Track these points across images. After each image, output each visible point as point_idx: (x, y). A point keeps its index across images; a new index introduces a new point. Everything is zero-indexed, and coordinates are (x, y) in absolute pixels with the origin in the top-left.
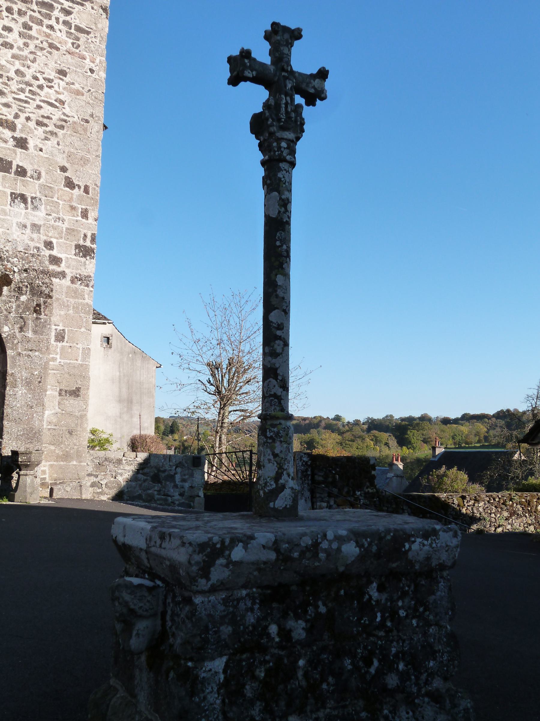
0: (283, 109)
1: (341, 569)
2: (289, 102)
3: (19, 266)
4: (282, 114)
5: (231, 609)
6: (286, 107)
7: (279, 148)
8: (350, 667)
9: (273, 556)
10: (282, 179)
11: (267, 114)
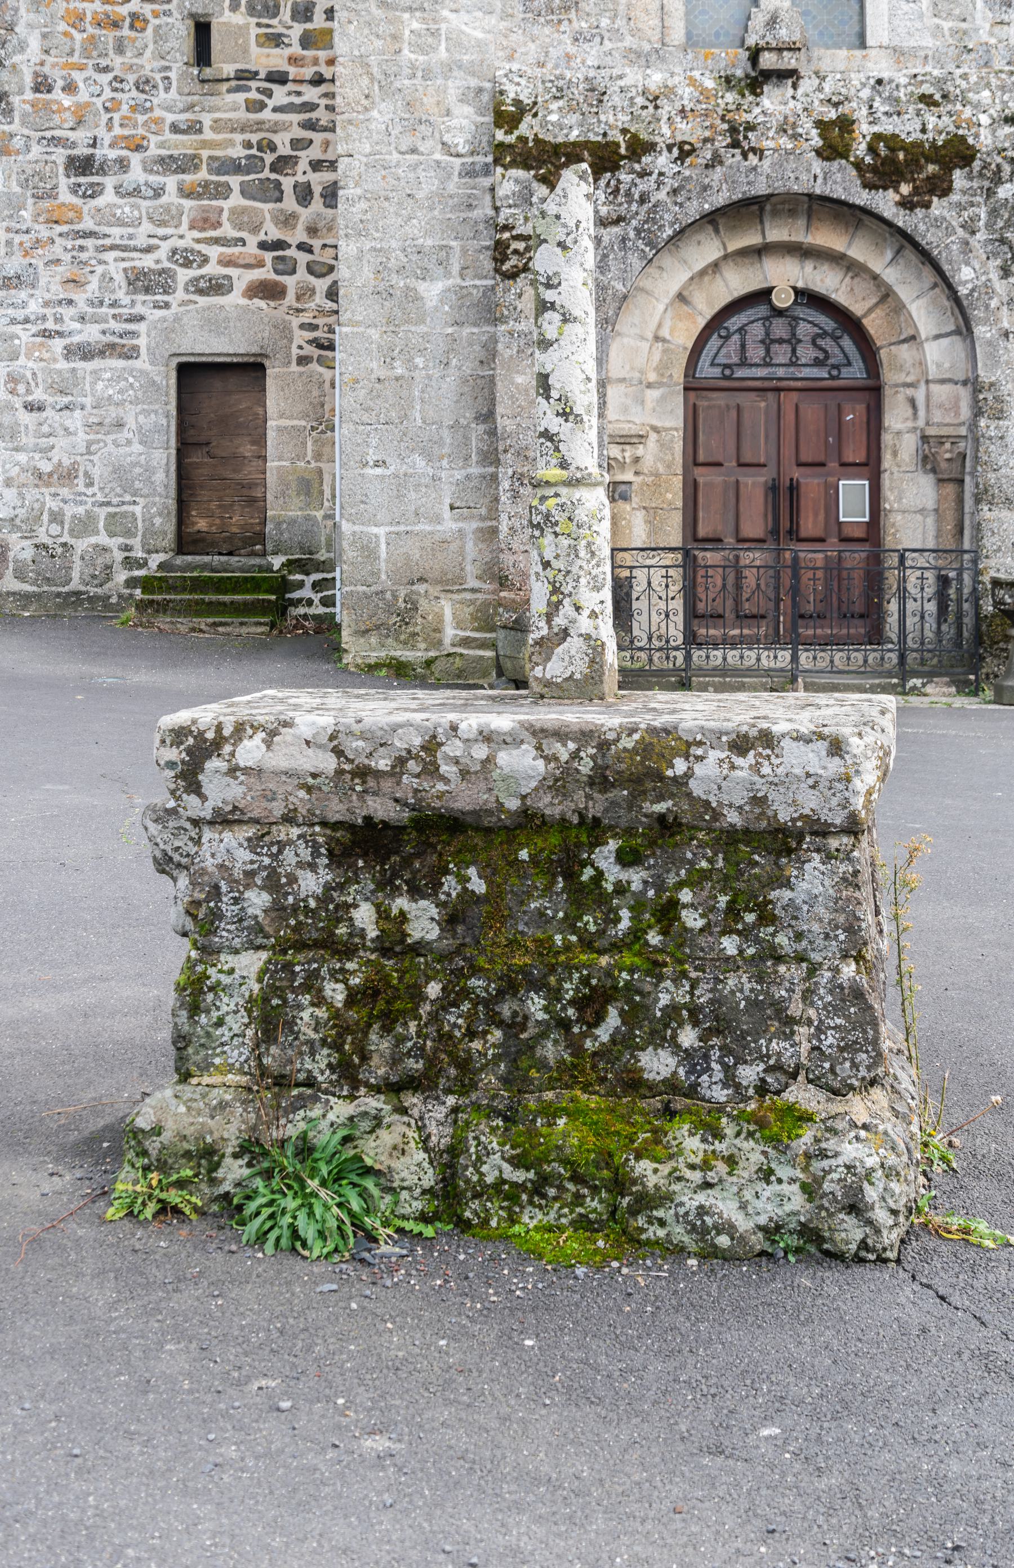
1: (513, 804)
3: (992, 111)
5: (267, 861)
8: (541, 1016)
9: (329, 763)
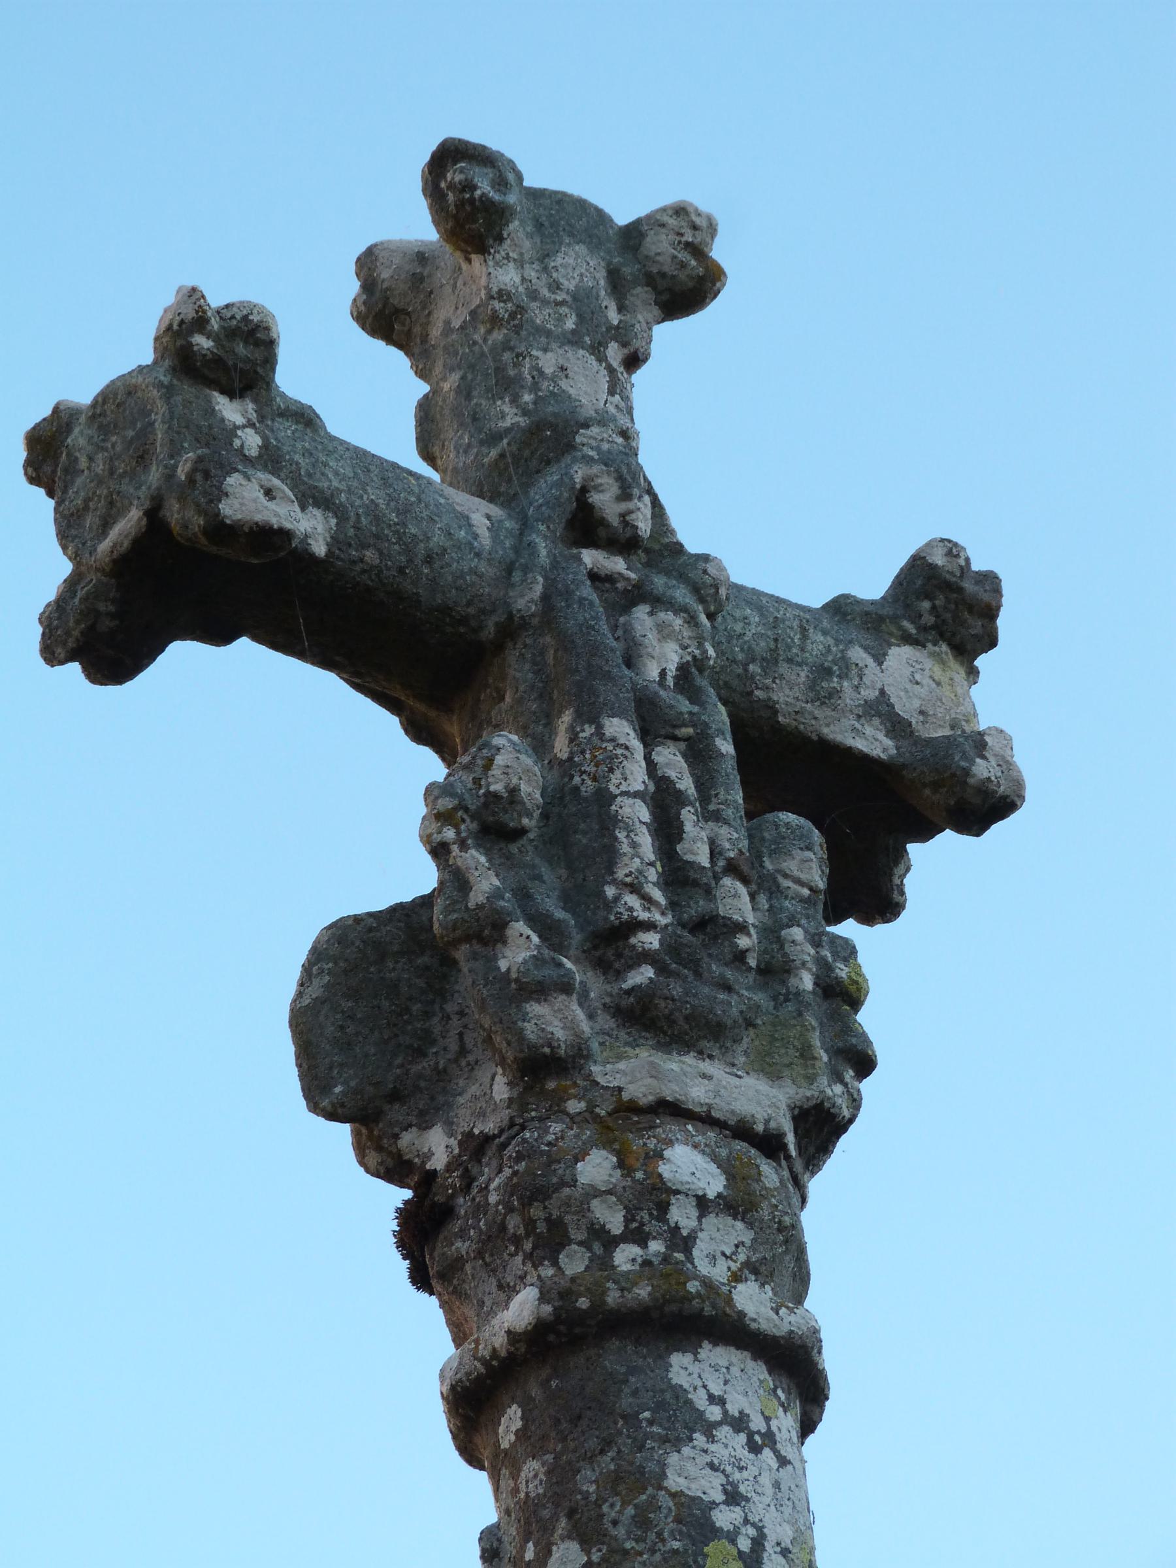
0: (639, 848)
2: (686, 784)
4: (635, 888)
6: (667, 831)
7: (651, 1198)
10: (725, 1518)
11: (486, 882)
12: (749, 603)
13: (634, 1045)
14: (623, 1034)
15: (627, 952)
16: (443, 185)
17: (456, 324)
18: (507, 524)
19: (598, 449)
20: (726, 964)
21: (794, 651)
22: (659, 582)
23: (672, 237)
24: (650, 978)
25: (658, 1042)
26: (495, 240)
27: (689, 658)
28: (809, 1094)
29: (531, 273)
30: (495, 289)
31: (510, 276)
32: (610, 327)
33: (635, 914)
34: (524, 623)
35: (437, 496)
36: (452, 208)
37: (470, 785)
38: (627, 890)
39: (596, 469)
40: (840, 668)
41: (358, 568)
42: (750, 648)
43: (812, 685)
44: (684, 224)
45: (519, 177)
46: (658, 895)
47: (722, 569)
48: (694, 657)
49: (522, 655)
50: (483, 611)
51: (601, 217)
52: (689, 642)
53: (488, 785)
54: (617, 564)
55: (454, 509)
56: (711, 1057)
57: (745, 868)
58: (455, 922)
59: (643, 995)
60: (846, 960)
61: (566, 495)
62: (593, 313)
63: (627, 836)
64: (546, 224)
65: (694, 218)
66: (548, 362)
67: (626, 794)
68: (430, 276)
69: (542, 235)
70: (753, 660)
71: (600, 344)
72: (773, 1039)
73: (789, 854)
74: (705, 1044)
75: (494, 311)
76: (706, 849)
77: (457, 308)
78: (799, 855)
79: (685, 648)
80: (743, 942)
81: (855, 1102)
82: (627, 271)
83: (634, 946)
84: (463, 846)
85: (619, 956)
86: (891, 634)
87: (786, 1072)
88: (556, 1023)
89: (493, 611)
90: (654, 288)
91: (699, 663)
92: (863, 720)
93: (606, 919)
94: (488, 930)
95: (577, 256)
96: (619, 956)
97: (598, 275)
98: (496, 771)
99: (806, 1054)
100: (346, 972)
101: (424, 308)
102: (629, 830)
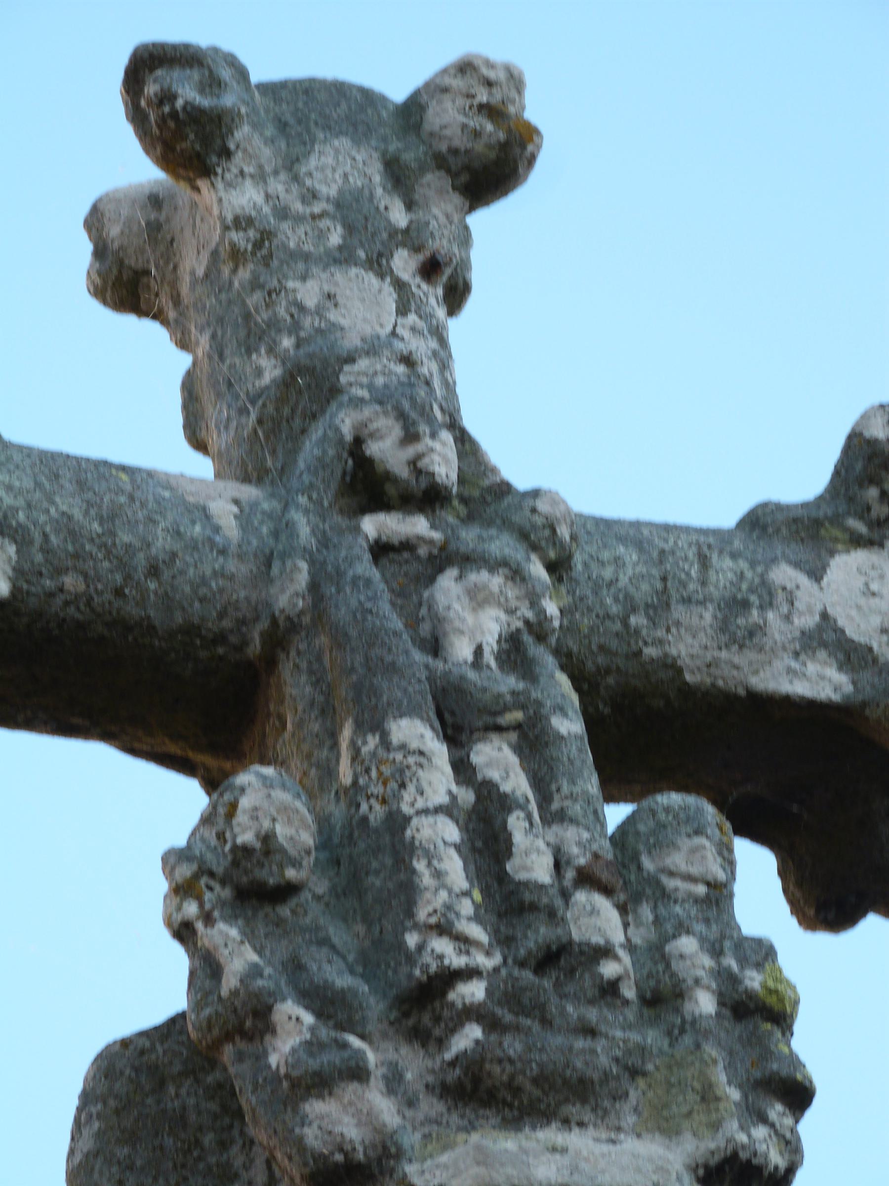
2: (516, 782)
4: (443, 929)
12: (622, 540)
13: (470, 1128)
14: (455, 1119)
15: (446, 1013)
16: (143, 103)
17: (200, 272)
18: (266, 506)
19: (371, 387)
20: (591, 1002)
21: (692, 586)
22: (469, 537)
23: (460, 101)
24: (477, 1042)
25: (504, 1119)
26: (219, 156)
27: (520, 624)
28: (712, 1146)
29: (277, 186)
30: (229, 217)
31: (248, 196)
32: (394, 232)
33: (446, 962)
34: (293, 625)
35: (159, 490)
36: (155, 130)
37: (214, 842)
38: (434, 933)
39: (367, 412)
40: (760, 597)
41: (59, 600)
42: (627, 595)
43: (724, 626)
44: (474, 82)
45: (242, 73)
46: (477, 932)
47: (555, 499)
48: (527, 622)
49: (297, 666)
50: (243, 622)
51: (369, 98)
52: (518, 604)
53: (234, 837)
54: (418, 526)
55: (184, 501)
56: (581, 1124)
57: (605, 876)
58: (209, 1020)
59: (472, 1065)
60: (759, 966)
61: (331, 452)
62: (366, 219)
63: (429, 864)
64: (291, 121)
65: (485, 71)
66: (309, 293)
67: (425, 812)
68: (168, 220)
69: (288, 137)
70: (634, 610)
71: (380, 255)
72: (670, 1085)
73: (674, 845)
74: (573, 1110)
75: (233, 245)
76: (547, 860)
77: (198, 253)
78: (685, 844)
79: (510, 612)
80: (609, 969)
81: (793, 1148)
82: (409, 157)
83: (453, 1004)
84: (208, 919)
85: (437, 1019)
86: (836, 540)
87: (686, 1124)
88: (346, 1119)
89: (257, 619)
90: (448, 171)
91: (538, 629)
92: (803, 657)
93: (410, 976)
94: (250, 1019)
95: (337, 152)
96: (437, 1019)
97: (369, 171)
98: (241, 818)
99: (708, 1096)
100: (117, 1112)
101: (167, 262)
102: (430, 857)
